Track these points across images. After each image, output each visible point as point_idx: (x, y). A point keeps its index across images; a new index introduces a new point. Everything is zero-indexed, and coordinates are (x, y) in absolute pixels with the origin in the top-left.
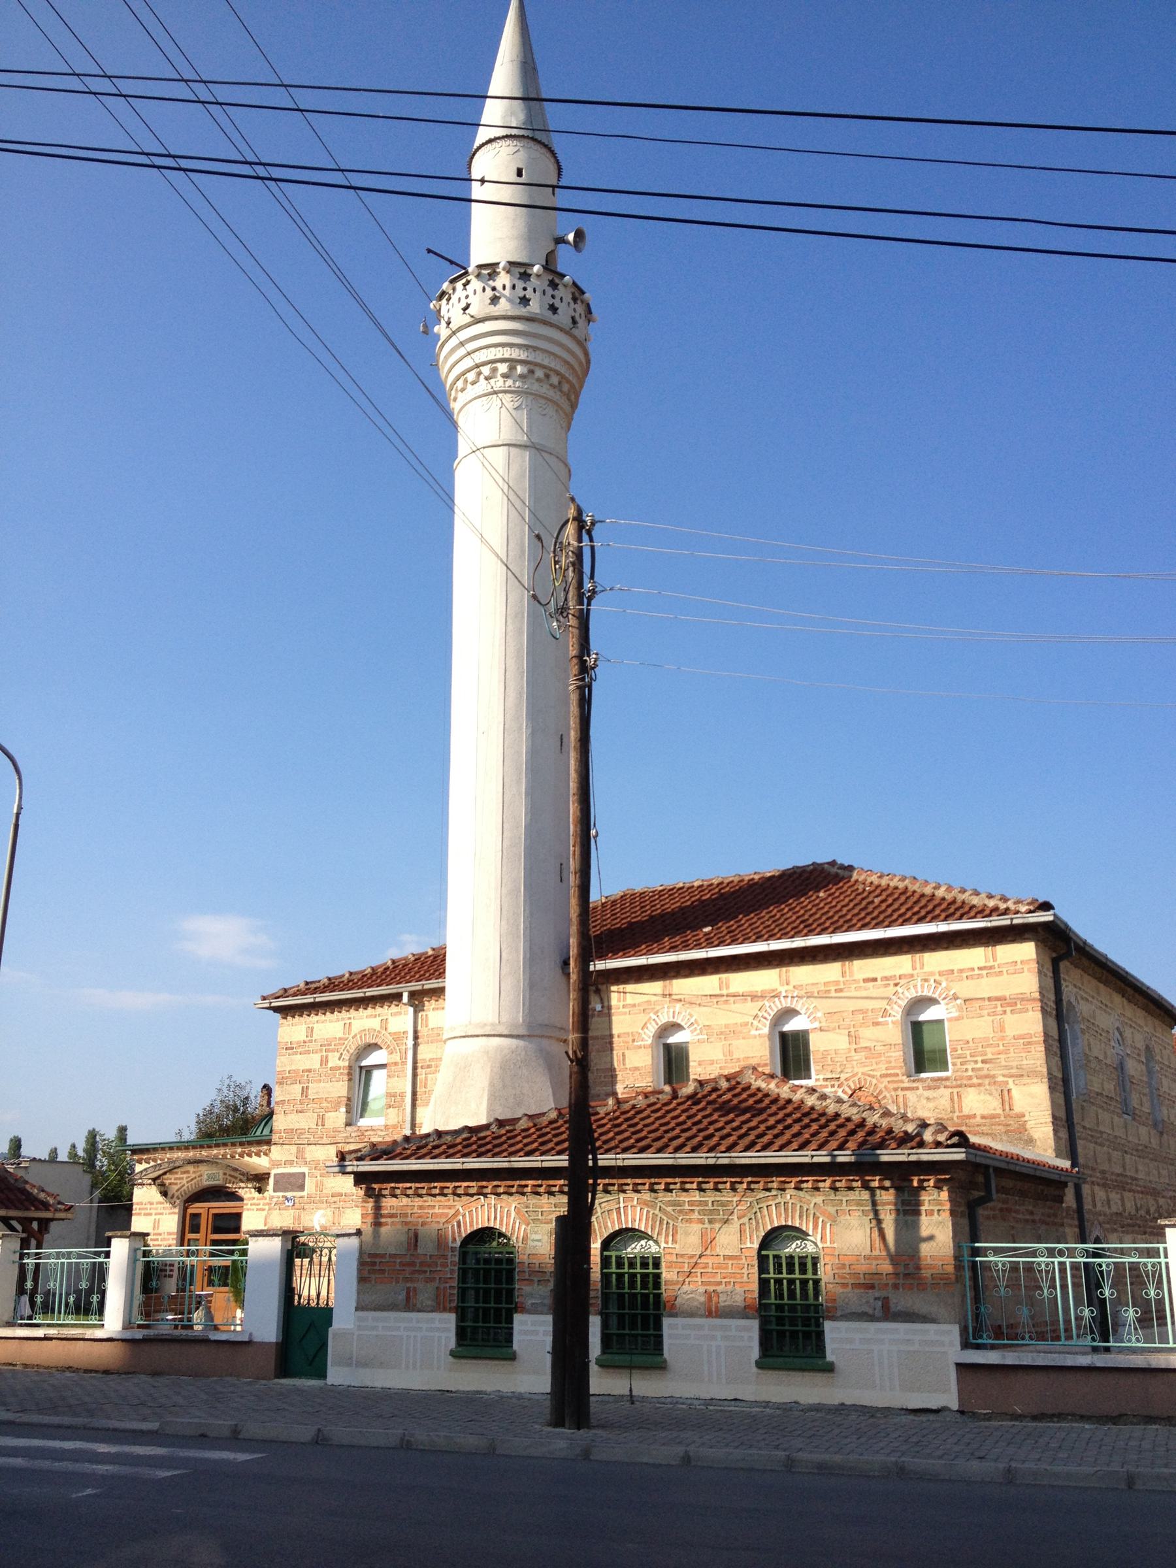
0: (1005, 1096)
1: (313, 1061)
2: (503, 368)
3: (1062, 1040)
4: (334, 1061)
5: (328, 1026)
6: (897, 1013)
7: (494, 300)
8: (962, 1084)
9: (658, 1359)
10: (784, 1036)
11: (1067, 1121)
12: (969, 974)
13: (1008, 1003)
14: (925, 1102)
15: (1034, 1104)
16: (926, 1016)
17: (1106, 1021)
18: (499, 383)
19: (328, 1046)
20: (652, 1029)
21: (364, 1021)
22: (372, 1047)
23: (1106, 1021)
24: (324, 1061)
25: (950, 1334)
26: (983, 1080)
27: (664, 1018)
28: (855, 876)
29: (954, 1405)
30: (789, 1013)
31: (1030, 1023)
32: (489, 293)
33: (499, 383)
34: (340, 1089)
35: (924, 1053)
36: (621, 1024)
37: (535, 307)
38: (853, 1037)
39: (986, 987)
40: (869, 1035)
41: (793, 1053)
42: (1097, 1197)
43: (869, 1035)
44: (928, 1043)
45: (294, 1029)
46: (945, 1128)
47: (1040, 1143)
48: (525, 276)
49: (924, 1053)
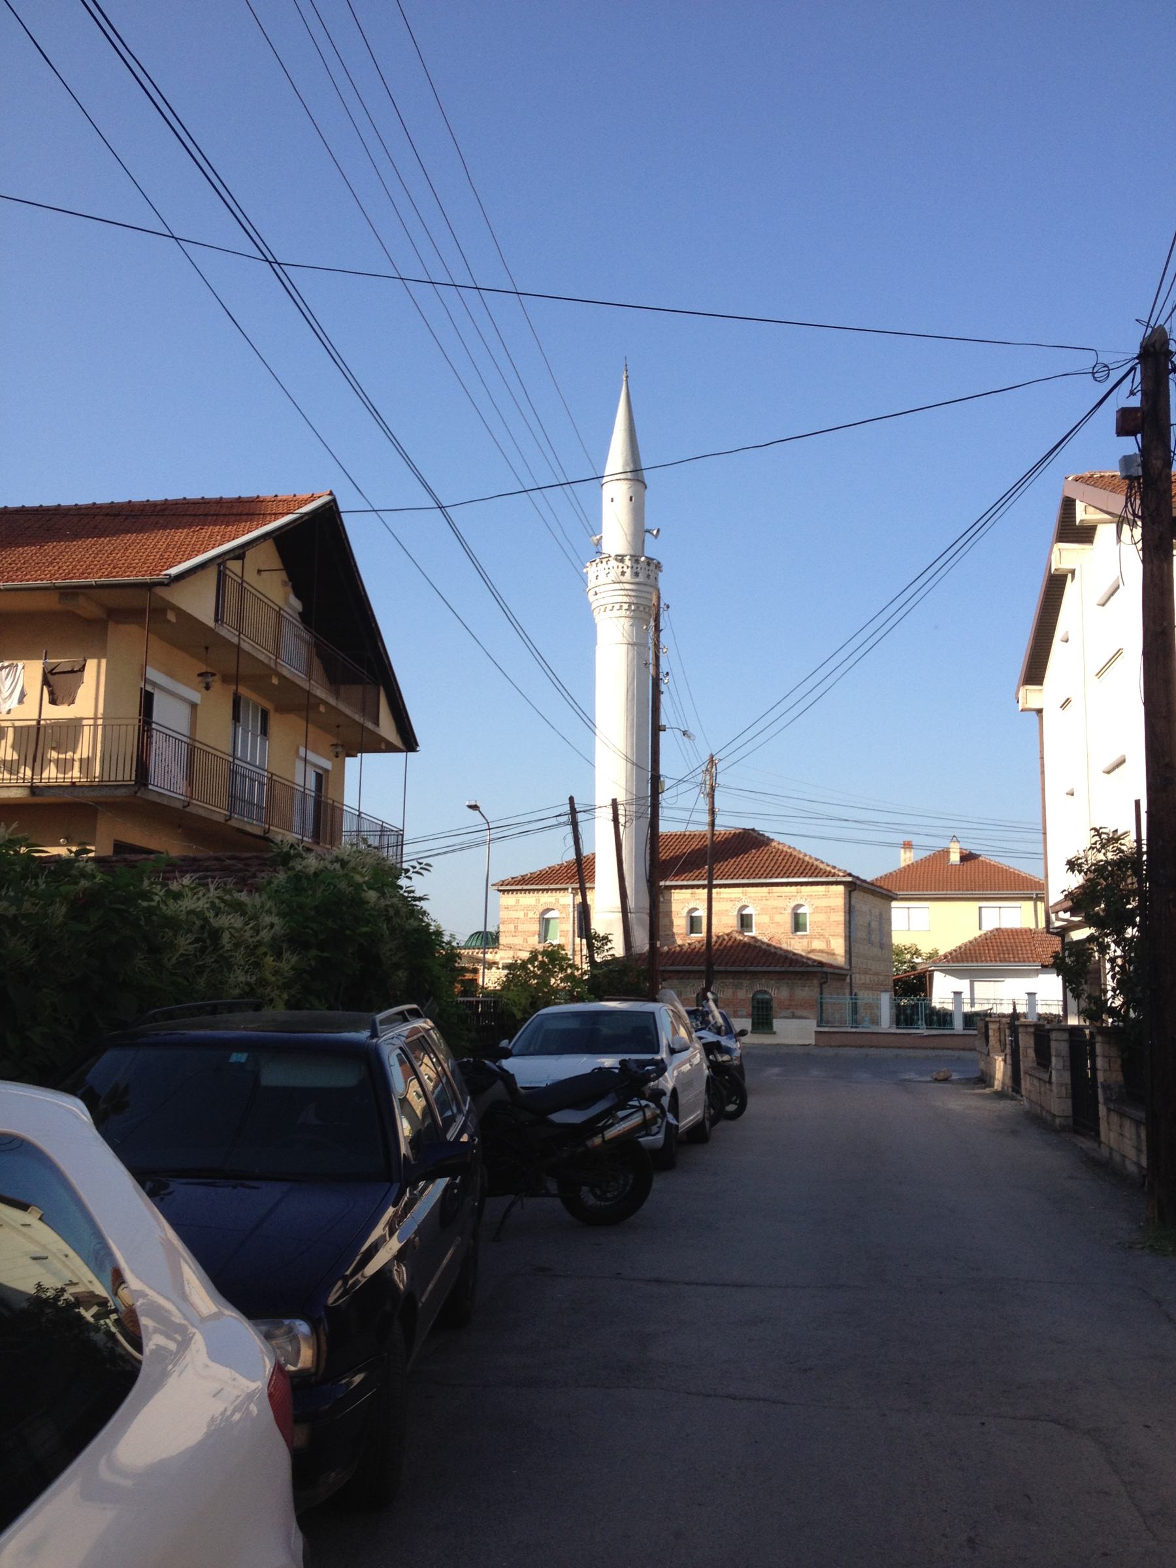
0: (828, 943)
1: (521, 915)
2: (625, 606)
3: (850, 922)
4: (531, 915)
5: (528, 899)
6: (789, 911)
7: (623, 573)
8: (812, 937)
9: (80, 1092)
10: (742, 916)
11: (849, 951)
12: (818, 897)
13: (832, 909)
14: (797, 945)
15: (838, 946)
16: (799, 911)
17: (865, 908)
18: (623, 613)
19: (527, 908)
20: (686, 910)
21: (546, 899)
22: (548, 910)
23: (865, 908)
24: (526, 915)
25: (814, 1022)
26: (821, 936)
27: (691, 906)
28: (773, 844)
29: (813, 1042)
30: (744, 907)
31: (840, 917)
32: (620, 570)
33: (623, 613)
34: (536, 927)
35: (798, 924)
36: (675, 907)
37: (640, 579)
38: (771, 919)
39: (824, 903)
40: (778, 918)
41: (745, 921)
42: (858, 979)
43: (778, 918)
44: (801, 920)
45: (509, 900)
46: (623, 556)
47: (840, 959)
48: (637, 561)
49: (798, 924)
